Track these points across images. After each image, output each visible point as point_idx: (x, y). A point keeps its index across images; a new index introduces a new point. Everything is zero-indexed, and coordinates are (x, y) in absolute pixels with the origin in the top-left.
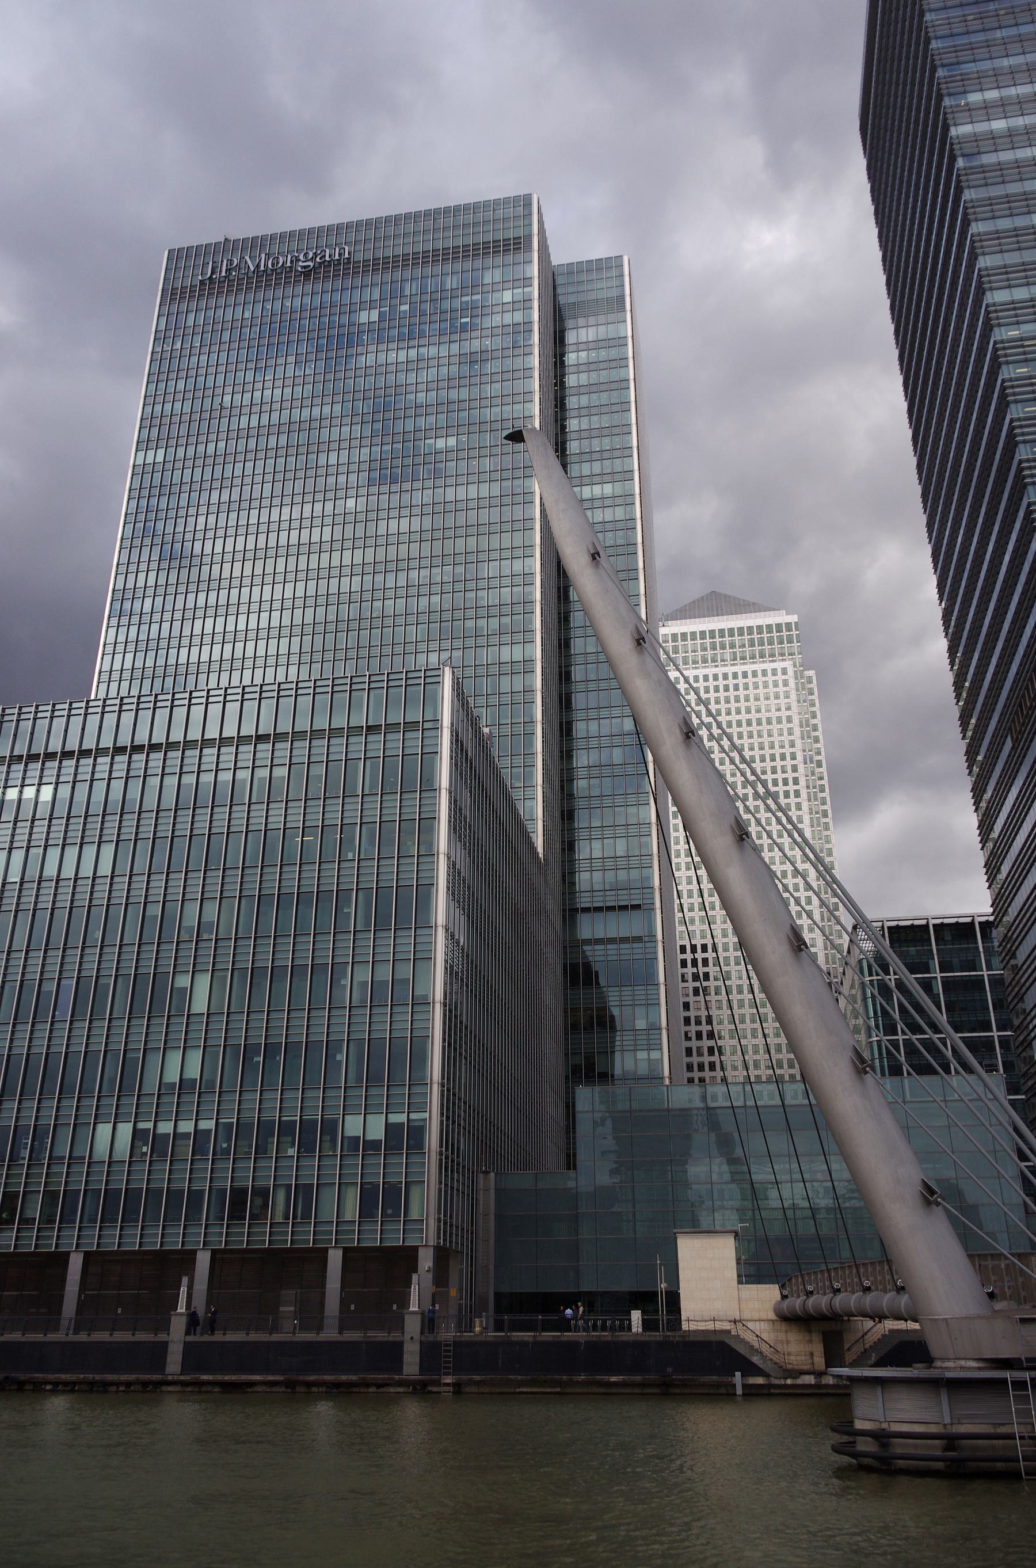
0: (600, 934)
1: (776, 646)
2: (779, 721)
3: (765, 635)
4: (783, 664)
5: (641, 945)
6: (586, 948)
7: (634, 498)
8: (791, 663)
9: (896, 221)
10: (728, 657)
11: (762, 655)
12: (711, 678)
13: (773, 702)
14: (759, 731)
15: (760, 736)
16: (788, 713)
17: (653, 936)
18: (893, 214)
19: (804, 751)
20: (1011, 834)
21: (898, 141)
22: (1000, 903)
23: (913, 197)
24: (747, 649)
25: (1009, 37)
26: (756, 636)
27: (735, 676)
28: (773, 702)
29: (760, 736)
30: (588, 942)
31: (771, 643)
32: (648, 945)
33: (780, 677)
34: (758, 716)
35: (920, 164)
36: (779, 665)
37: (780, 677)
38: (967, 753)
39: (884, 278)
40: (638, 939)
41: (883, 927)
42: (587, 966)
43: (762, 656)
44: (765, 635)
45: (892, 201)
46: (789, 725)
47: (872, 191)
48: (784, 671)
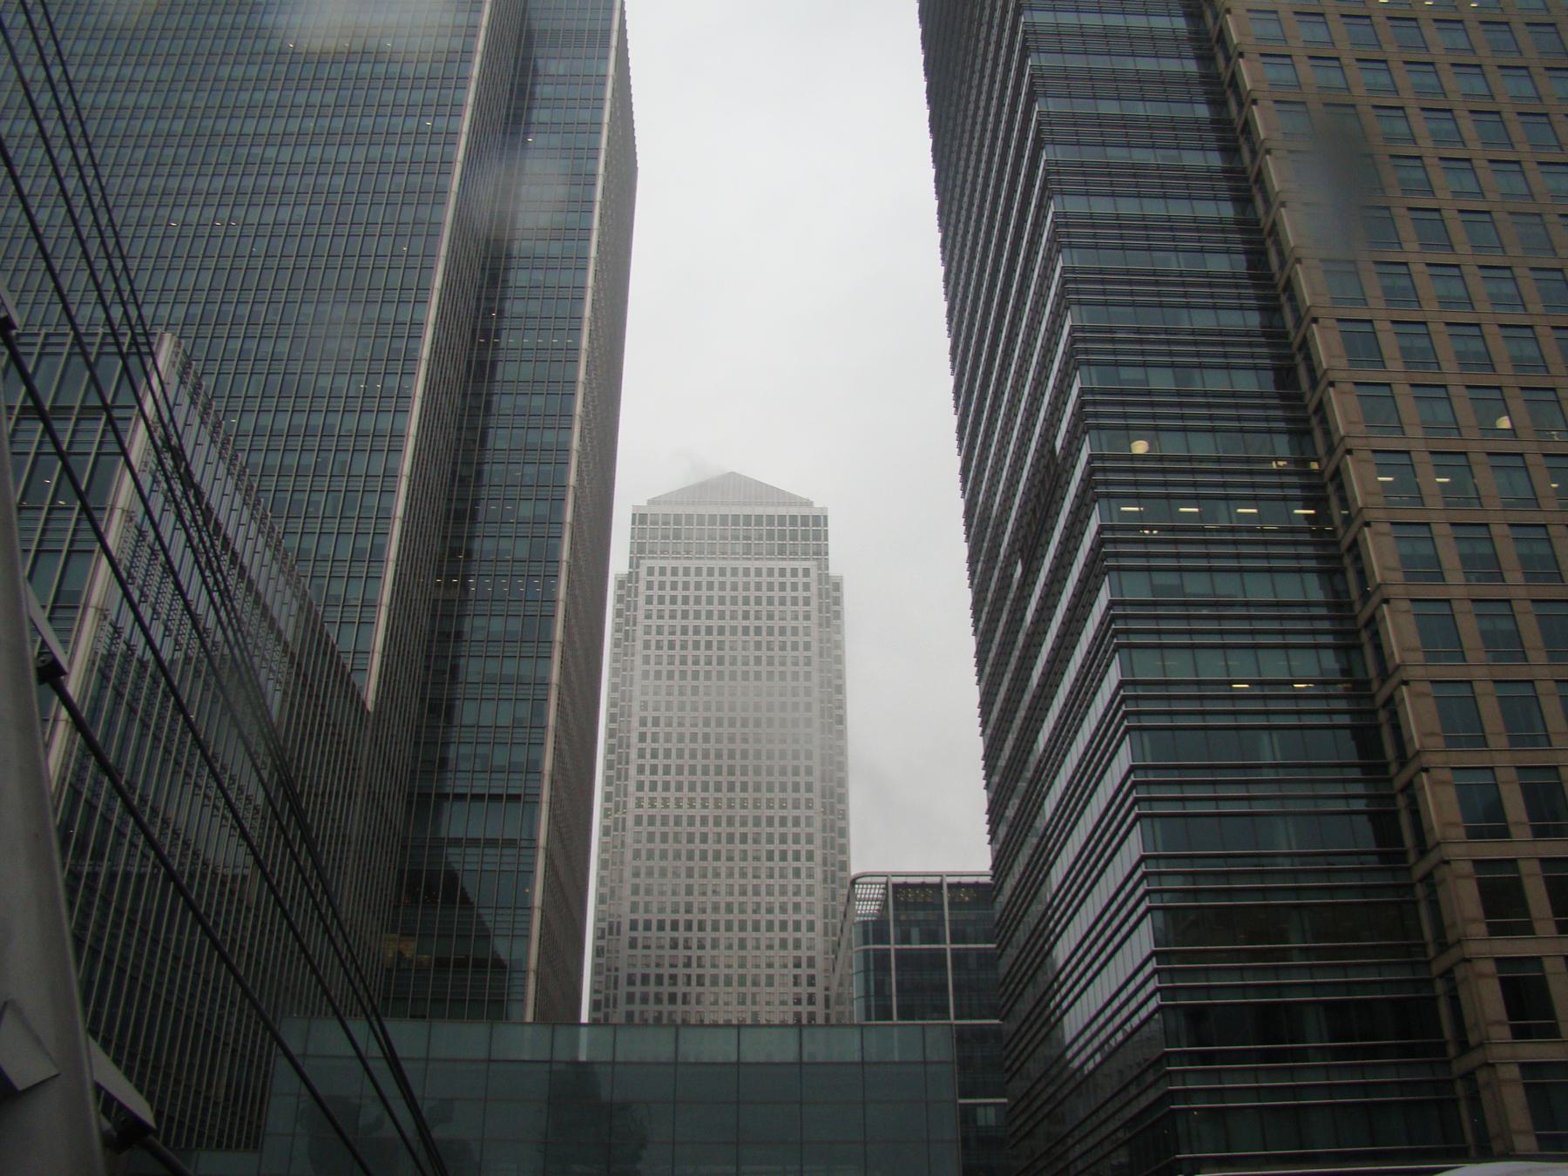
0: (476, 832)
1: (799, 542)
2: (795, 601)
3: (788, 528)
4: (806, 564)
5: (514, 851)
6: (451, 850)
7: (593, 206)
8: (815, 563)
9: (974, 183)
10: (740, 549)
11: (782, 552)
12: (717, 572)
13: (789, 608)
14: (769, 643)
15: (770, 648)
16: (806, 623)
17: (533, 840)
18: (991, 119)
19: (822, 702)
20: (1095, 770)
21: (996, 59)
22: (1001, 862)
23: (1013, 87)
24: (765, 542)
25: (1066, 164)
26: (776, 528)
27: (711, 572)
28: (789, 608)
29: (770, 648)
30: (456, 842)
31: (794, 538)
32: (524, 852)
33: (800, 579)
34: (770, 623)
35: (1000, 180)
36: (800, 565)
37: (800, 579)
38: (990, 811)
39: (944, 306)
40: (510, 843)
41: (887, 884)
42: (452, 878)
43: (781, 552)
44: (788, 528)
45: (995, 65)
46: (805, 580)
47: (941, 212)
48: (806, 572)
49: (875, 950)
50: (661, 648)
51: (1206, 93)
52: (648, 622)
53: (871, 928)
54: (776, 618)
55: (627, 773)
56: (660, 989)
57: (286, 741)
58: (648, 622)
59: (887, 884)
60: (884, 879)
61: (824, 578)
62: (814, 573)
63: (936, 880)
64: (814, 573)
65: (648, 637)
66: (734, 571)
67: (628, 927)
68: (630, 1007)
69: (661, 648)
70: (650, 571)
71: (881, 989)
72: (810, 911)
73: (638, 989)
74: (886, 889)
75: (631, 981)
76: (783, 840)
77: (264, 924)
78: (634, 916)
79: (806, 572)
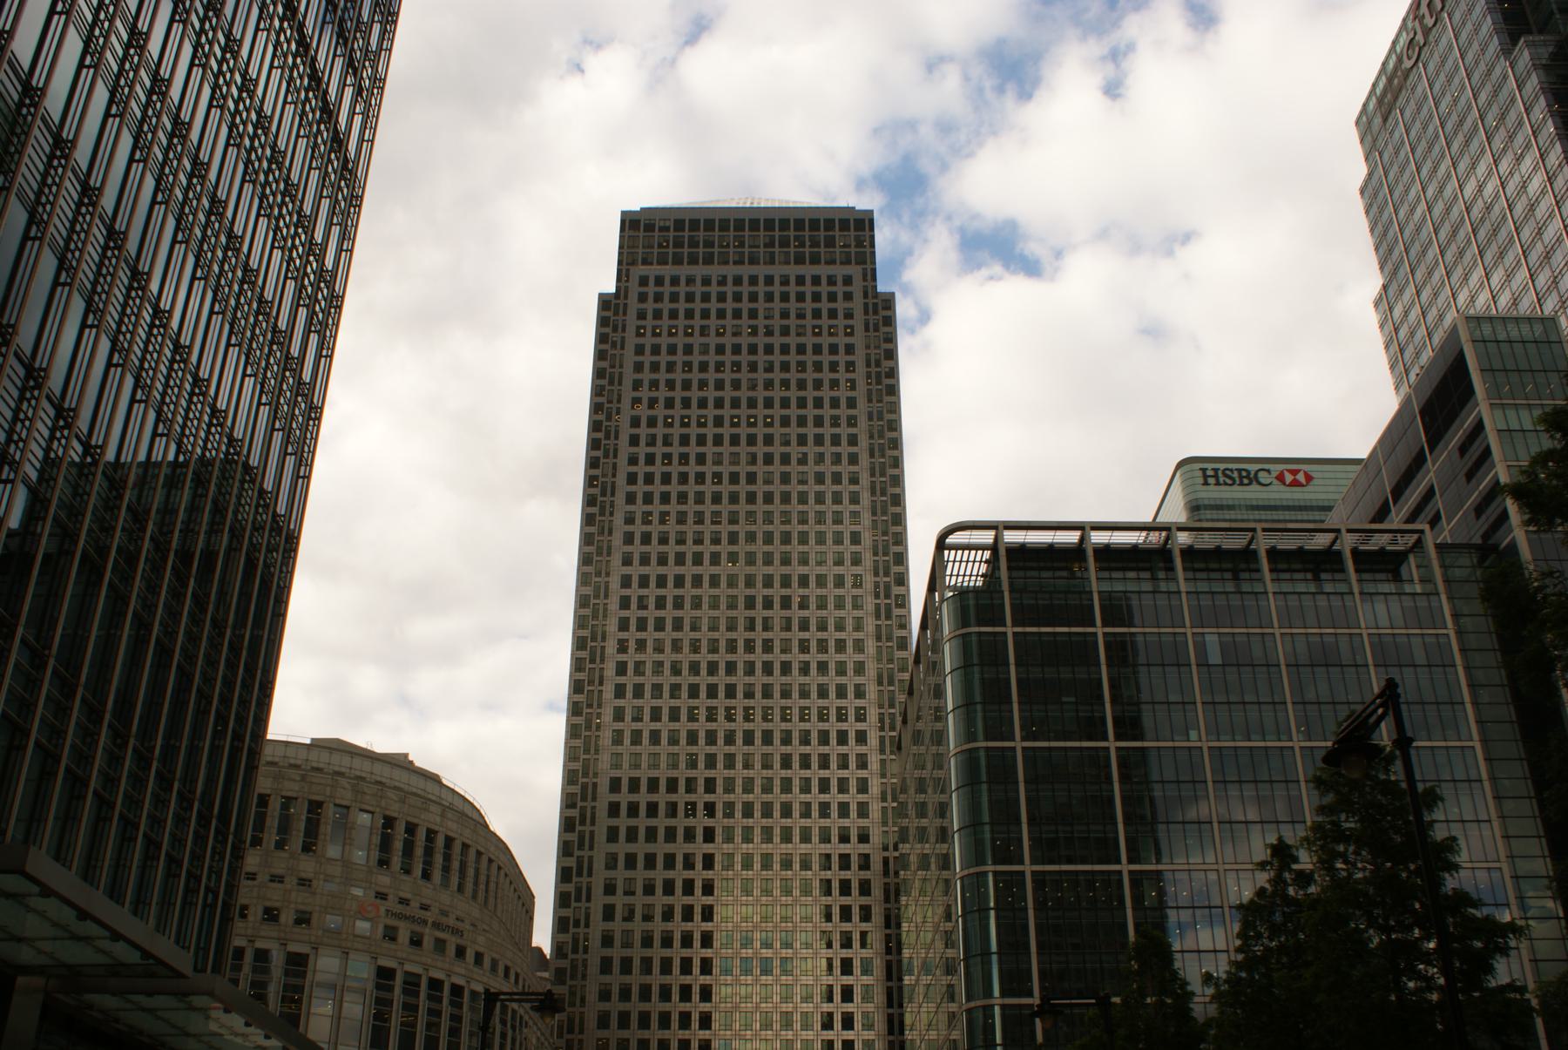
27: (690, 281)
33: (840, 289)
36: (839, 271)
37: (840, 289)
48: (848, 281)
49: (987, 749)
50: (646, 608)
51: (1550, 83)
52: (627, 570)
53: (972, 602)
54: (812, 562)
55: (607, 588)
56: (647, 979)
57: (337, 43)
58: (627, 570)
59: (994, 548)
60: (987, 537)
61: (870, 291)
62: (857, 288)
63: (1072, 537)
64: (857, 288)
65: (626, 592)
66: (832, 281)
67: (604, 838)
68: (614, 822)
69: (646, 608)
70: (644, 281)
71: (1005, 814)
72: (856, 607)
73: (624, 798)
74: (993, 563)
75: (615, 785)
76: (822, 605)
77: (218, 626)
78: (616, 773)
79: (848, 281)
